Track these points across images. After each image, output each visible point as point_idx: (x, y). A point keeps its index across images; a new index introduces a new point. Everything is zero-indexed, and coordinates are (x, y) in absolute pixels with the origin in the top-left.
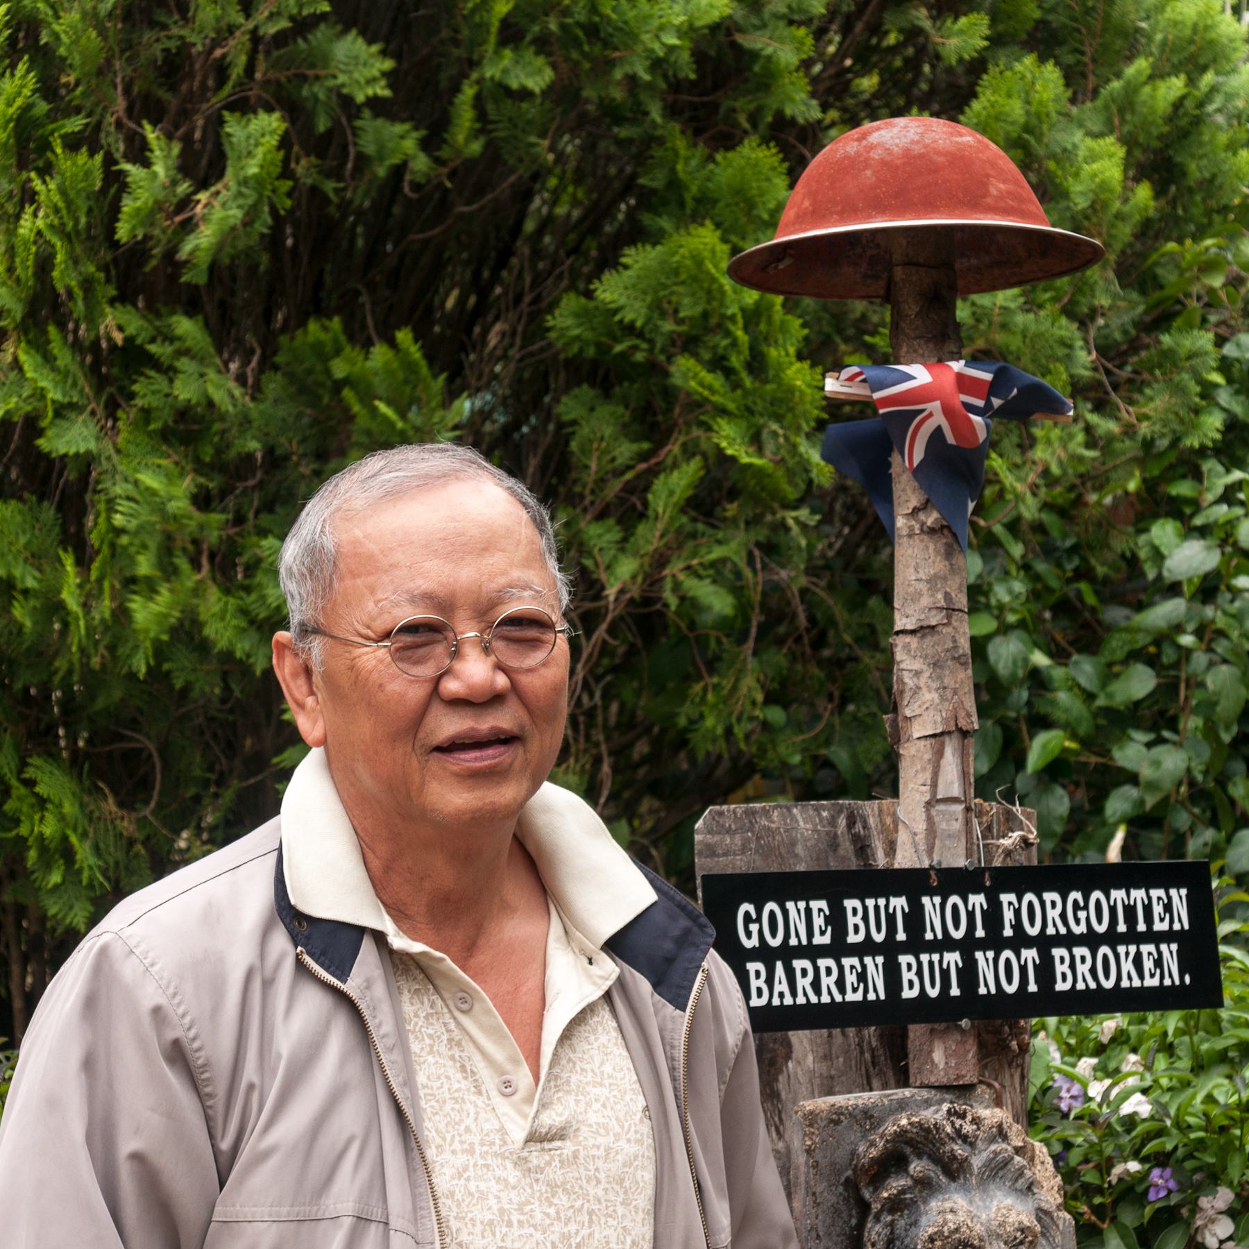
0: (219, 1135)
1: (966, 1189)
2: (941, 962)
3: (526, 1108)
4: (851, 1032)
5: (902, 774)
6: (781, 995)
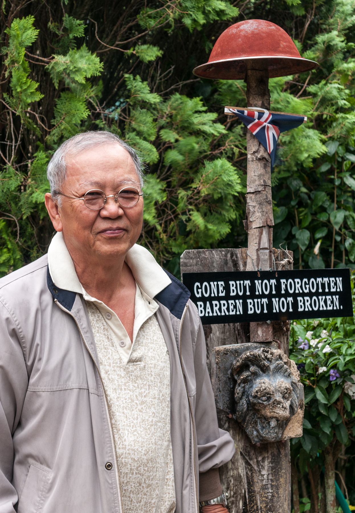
0: (27, 360)
1: (268, 376)
2: (261, 302)
3: (128, 351)
4: (231, 324)
5: (249, 240)
6: (209, 313)
